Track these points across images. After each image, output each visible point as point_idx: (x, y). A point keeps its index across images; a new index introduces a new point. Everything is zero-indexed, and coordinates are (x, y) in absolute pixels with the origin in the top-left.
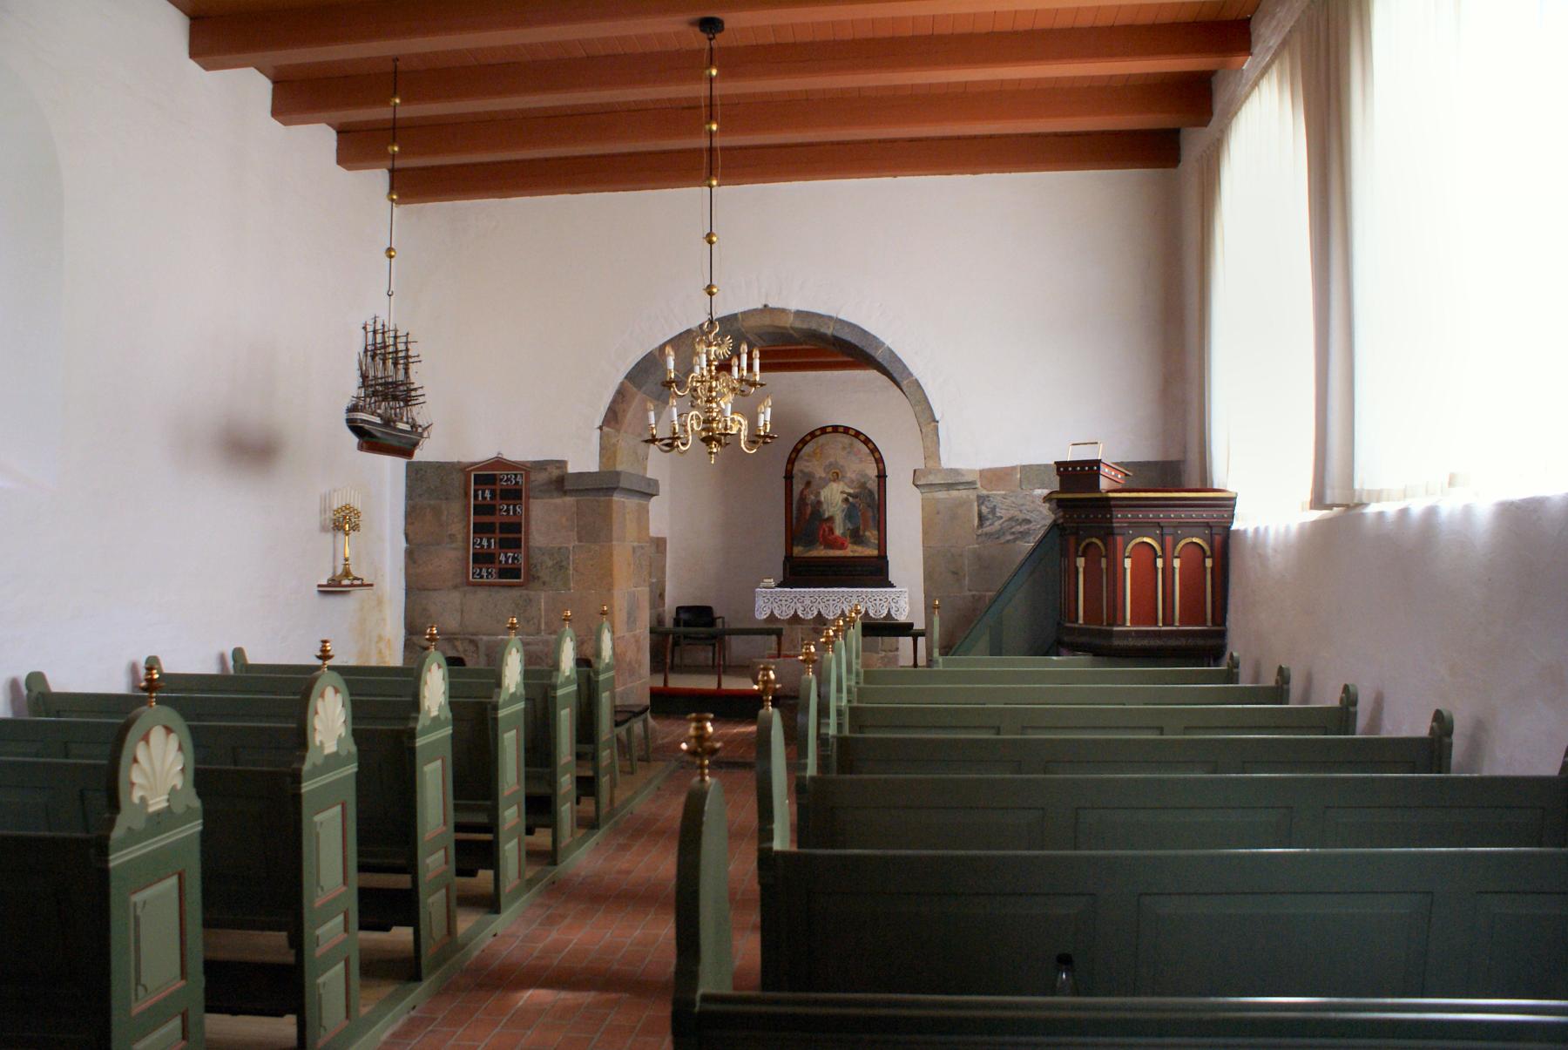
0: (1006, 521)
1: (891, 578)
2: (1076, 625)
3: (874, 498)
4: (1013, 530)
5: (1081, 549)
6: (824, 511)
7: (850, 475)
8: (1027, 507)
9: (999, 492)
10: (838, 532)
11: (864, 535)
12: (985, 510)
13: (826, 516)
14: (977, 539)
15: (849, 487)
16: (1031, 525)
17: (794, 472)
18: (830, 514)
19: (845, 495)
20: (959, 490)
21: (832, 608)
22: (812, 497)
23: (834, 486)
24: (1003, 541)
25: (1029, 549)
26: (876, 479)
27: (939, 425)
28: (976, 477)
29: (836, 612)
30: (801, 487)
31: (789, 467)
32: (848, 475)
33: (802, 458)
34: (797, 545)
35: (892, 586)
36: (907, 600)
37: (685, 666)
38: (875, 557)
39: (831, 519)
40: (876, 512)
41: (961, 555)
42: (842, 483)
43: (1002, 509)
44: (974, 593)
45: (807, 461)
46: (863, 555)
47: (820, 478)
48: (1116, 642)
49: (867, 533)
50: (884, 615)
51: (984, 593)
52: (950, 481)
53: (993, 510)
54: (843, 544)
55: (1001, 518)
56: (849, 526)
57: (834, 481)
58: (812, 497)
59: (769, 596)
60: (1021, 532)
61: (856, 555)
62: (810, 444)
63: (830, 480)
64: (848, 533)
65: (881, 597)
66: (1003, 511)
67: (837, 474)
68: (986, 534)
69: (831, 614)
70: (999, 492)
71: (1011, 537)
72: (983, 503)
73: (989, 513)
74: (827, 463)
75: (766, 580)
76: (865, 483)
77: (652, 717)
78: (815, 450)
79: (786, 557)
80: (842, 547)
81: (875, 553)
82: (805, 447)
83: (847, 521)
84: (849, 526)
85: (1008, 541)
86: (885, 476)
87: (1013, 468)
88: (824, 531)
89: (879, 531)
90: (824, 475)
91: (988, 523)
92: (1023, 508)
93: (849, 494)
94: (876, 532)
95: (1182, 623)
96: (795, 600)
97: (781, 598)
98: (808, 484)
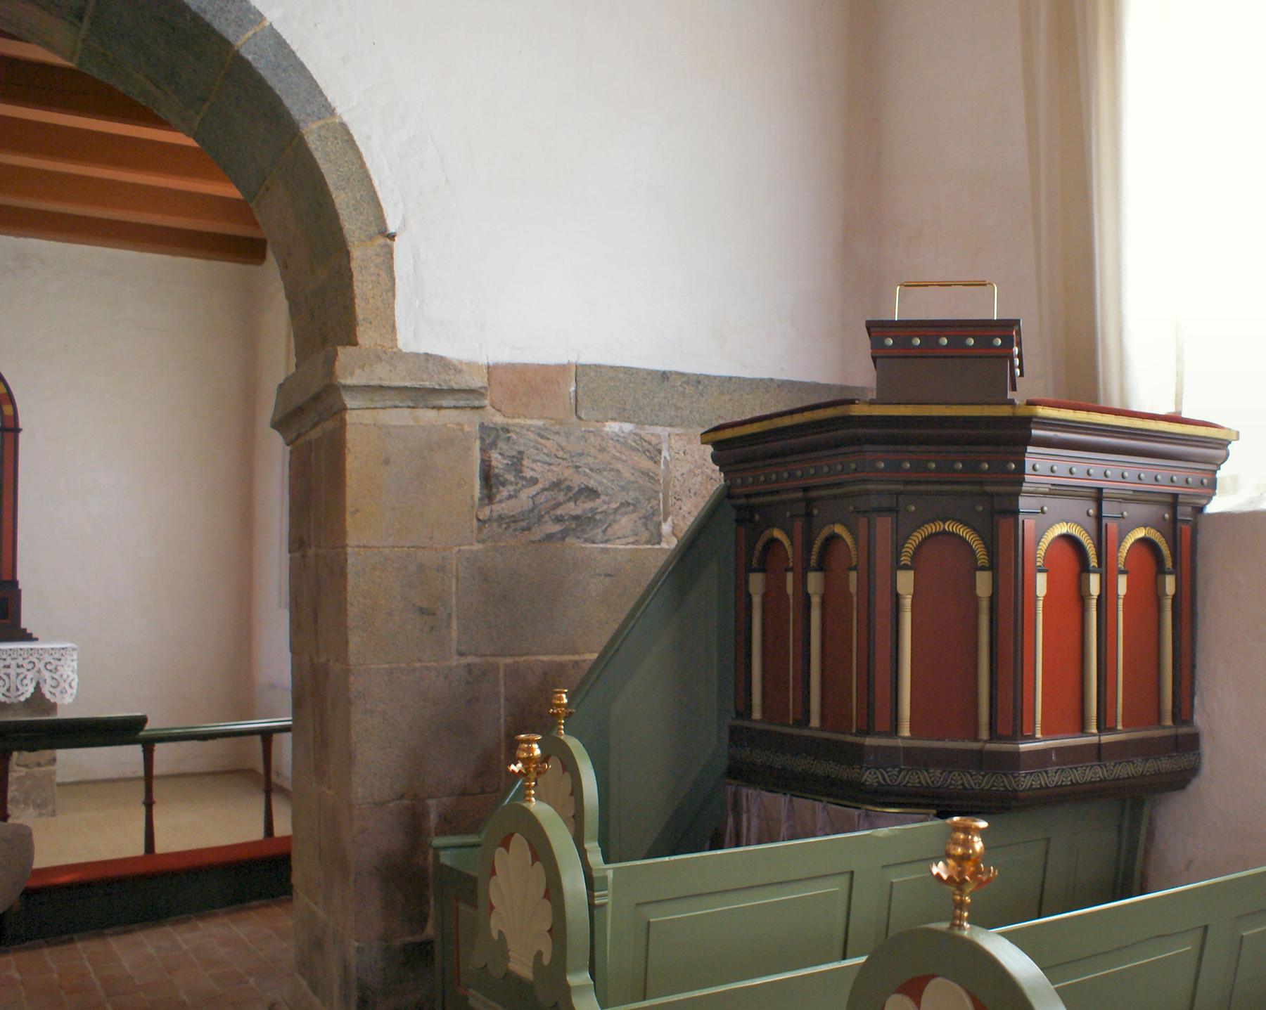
0: (544, 490)
1: (26, 622)
2: (805, 732)
4: (559, 512)
5: (814, 558)
8: (591, 460)
9: (529, 422)
12: (498, 461)
14: (480, 530)
16: (598, 501)
20: (440, 408)
24: (537, 538)
25: (662, 559)
27: (398, 246)
28: (478, 382)
35: (28, 637)
36: (75, 664)
41: (441, 569)
43: (535, 461)
44: (470, 659)
48: (1027, 780)
50: (28, 695)
51: (491, 659)
52: (428, 384)
53: (516, 463)
55: (534, 481)
60: (576, 518)
65: (20, 661)
66: (538, 466)
68: (501, 518)
70: (529, 422)
71: (556, 528)
72: (494, 445)
73: (507, 468)
85: (550, 537)
87: (563, 369)
91: (504, 492)
92: (583, 461)
95: (1048, 732)
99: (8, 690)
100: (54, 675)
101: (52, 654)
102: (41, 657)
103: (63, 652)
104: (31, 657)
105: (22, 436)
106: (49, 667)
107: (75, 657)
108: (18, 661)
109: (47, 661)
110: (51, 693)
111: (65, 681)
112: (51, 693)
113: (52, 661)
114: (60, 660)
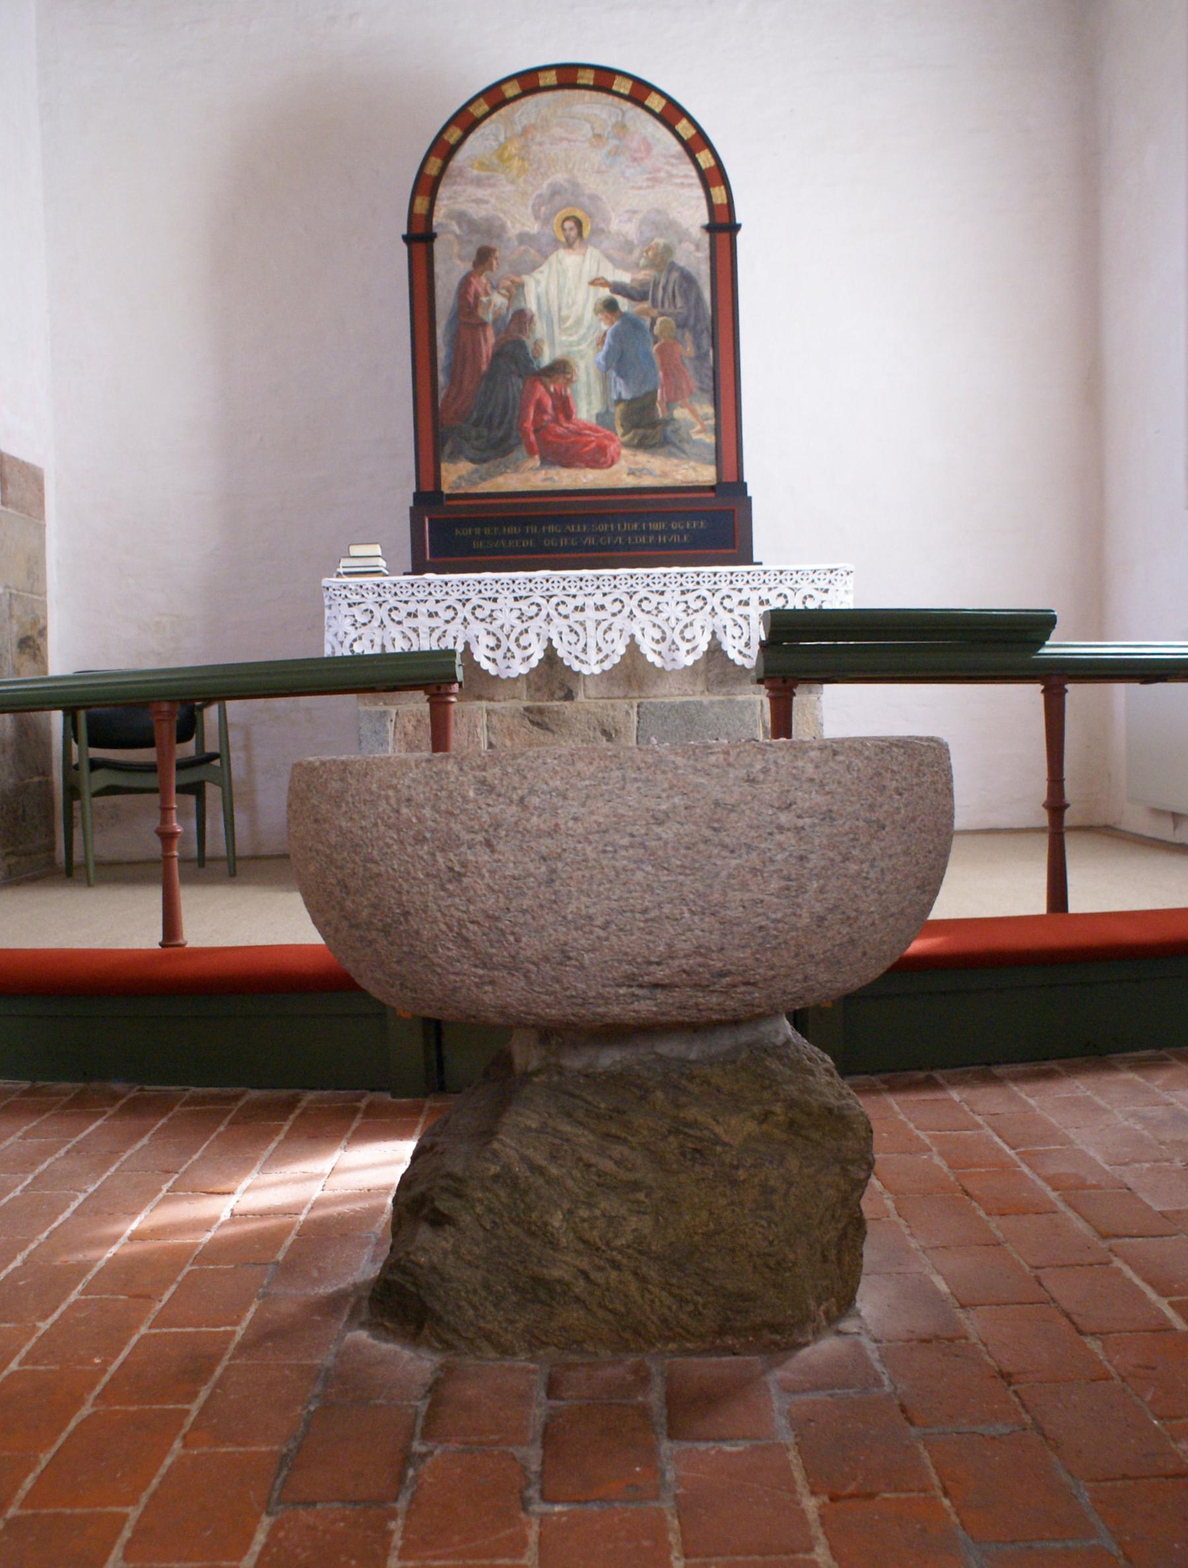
3: (699, 298)
6: (538, 345)
7: (623, 226)
10: (587, 409)
11: (671, 420)
13: (546, 360)
15: (618, 264)
17: (436, 220)
18: (559, 353)
19: (605, 293)
21: (593, 636)
22: (499, 300)
23: (568, 260)
26: (705, 239)
29: (606, 649)
30: (465, 267)
31: (421, 205)
32: (614, 226)
33: (461, 173)
34: (454, 457)
37: (100, 864)
38: (712, 488)
39: (561, 368)
40: (706, 341)
42: (592, 253)
45: (479, 182)
46: (667, 482)
47: (524, 238)
49: (680, 413)
54: (602, 449)
56: (622, 389)
57: (569, 245)
58: (499, 300)
59: (370, 600)
61: (647, 482)
62: (486, 128)
63: (555, 244)
64: (618, 411)
67: (579, 224)
69: (593, 656)
74: (544, 188)
75: (355, 550)
76: (668, 250)
77: (765, 612)
78: (503, 147)
79: (419, 497)
80: (599, 458)
81: (706, 475)
82: (472, 138)
83: (613, 374)
84: (622, 389)
86: (734, 228)
88: (540, 408)
89: (716, 405)
90: (534, 228)
93: (618, 288)
94: (709, 410)
96: (464, 612)
97: (411, 607)
98: (484, 257)
99: (747, 645)
100: (490, 628)
101: (396, 594)
102: (797, 586)
103: (829, 576)
104: (780, 586)
105: (740, 237)
106: (478, 612)
107: (850, 587)
108: (760, 593)
109: (807, 593)
110: (488, 658)
111: (508, 636)
112: (655, 651)
113: (814, 593)
114: (826, 591)
